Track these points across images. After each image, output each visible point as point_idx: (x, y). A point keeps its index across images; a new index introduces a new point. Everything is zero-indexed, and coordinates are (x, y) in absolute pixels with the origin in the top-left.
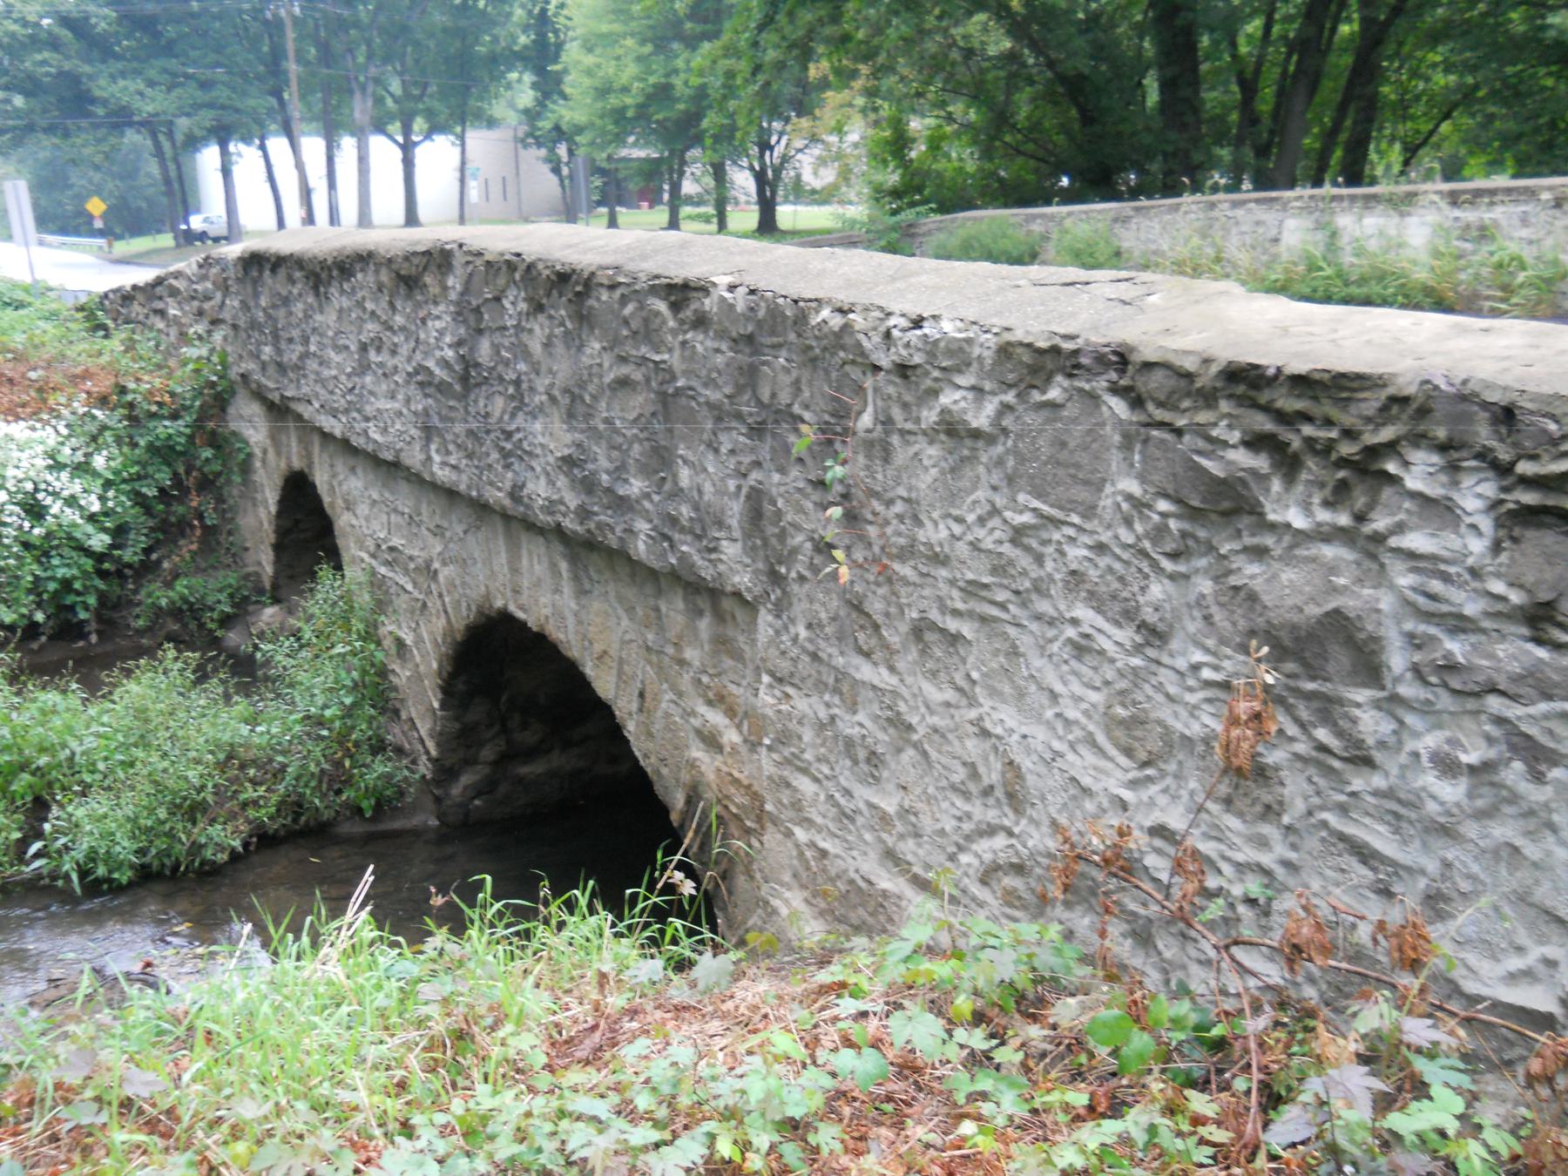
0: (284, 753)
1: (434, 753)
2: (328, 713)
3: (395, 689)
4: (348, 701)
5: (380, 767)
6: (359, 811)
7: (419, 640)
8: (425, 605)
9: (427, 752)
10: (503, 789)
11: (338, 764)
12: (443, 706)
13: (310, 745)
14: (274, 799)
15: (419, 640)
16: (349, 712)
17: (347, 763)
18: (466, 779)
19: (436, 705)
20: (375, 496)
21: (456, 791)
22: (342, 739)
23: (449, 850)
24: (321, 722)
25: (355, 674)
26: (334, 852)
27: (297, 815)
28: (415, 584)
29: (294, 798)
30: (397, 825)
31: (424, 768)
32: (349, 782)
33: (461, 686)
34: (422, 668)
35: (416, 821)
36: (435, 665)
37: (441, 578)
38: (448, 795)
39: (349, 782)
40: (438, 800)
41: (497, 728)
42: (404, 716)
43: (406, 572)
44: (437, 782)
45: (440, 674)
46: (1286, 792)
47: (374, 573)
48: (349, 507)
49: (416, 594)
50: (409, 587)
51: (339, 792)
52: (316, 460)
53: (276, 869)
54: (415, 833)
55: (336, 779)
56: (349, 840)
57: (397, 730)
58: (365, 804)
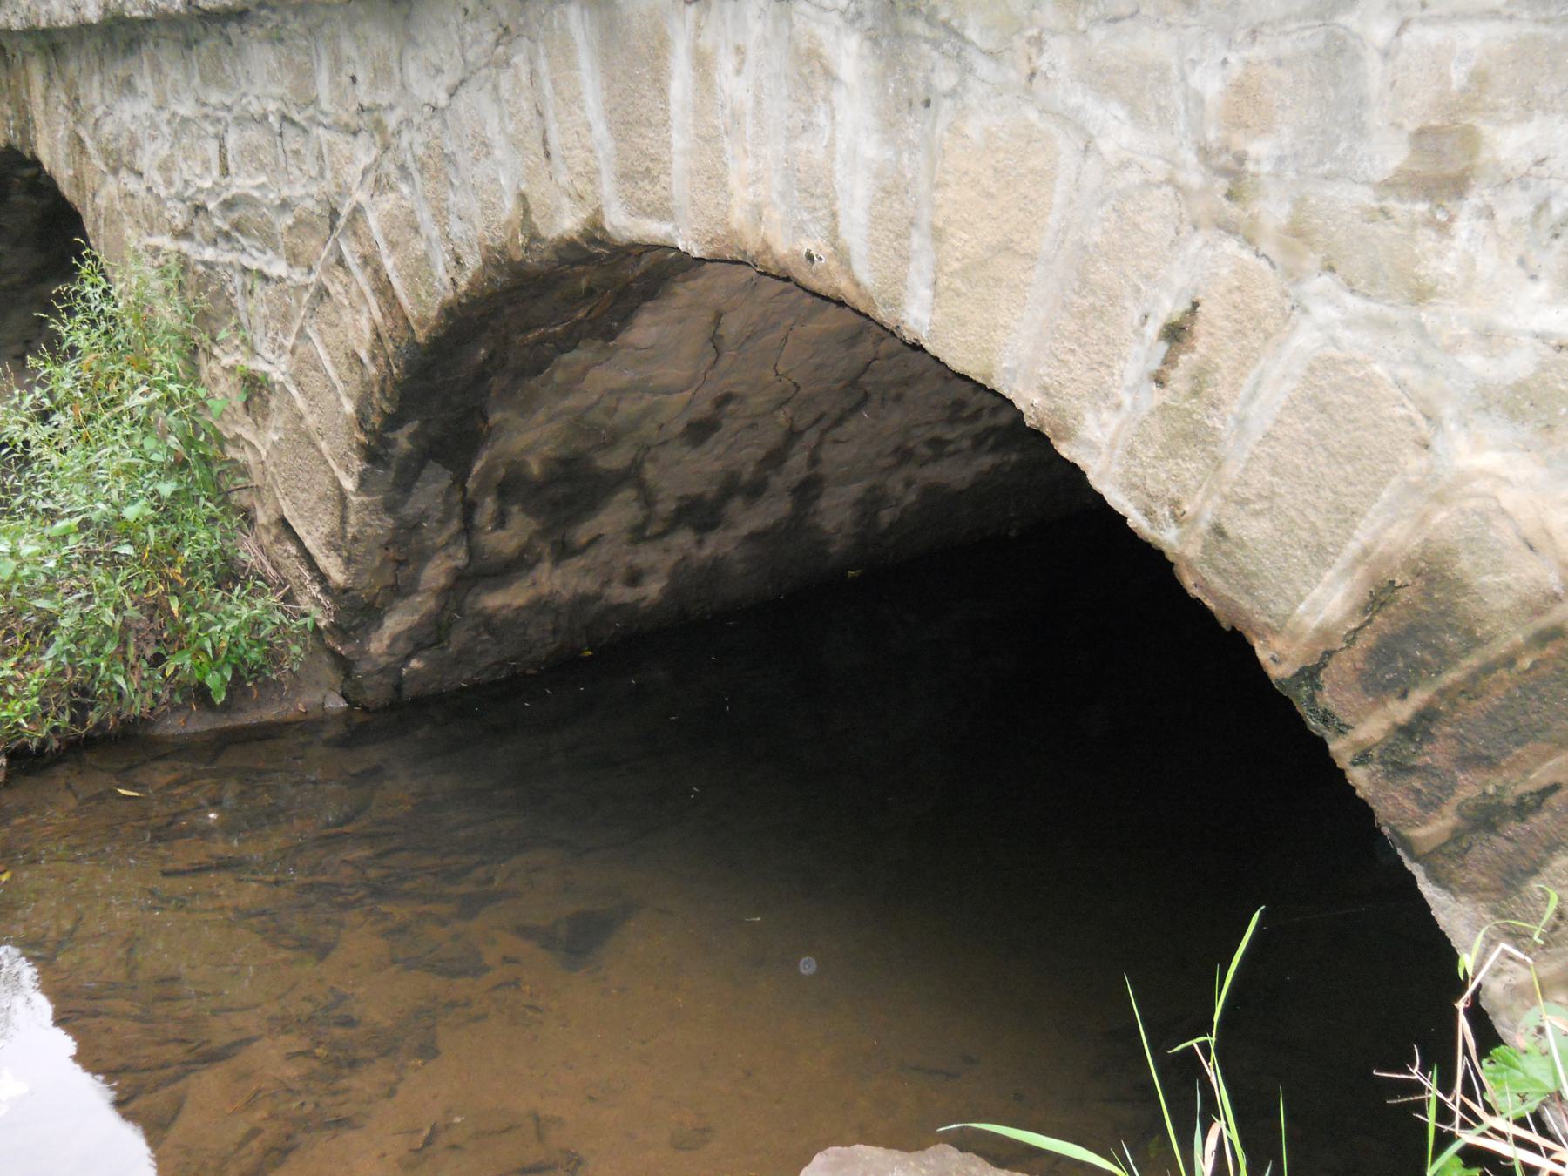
0: (49, 594)
1: (338, 576)
2: (130, 512)
3: (244, 471)
4: (166, 489)
5: (242, 609)
6: (202, 693)
7: (305, 366)
8: (322, 293)
9: (322, 578)
10: (458, 638)
11: (156, 608)
12: (363, 483)
13: (99, 576)
14: (35, 681)
15: (305, 366)
16: (166, 512)
17: (175, 605)
18: (396, 622)
19: (349, 484)
20: (186, 109)
21: (378, 645)
22: (161, 559)
23: (373, 754)
24: (114, 529)
25: (172, 441)
26: (160, 775)
27: (80, 712)
28: (293, 258)
29: (70, 678)
30: (271, 714)
31: (316, 610)
32: (177, 640)
33: (403, 440)
34: (311, 421)
35: (303, 703)
36: (349, 407)
37: (373, 221)
38: (364, 653)
39: (177, 640)
40: (344, 665)
41: (455, 525)
42: (262, 518)
43: (268, 240)
44: (340, 630)
45: (362, 420)
46: (545, 566)
47: (185, 265)
48: (117, 163)
49: (298, 276)
50: (278, 269)
51: (158, 660)
52: (37, 113)
53: (57, 816)
54: (309, 725)
55: (159, 635)
56: (183, 749)
57: (250, 543)
58: (213, 681)
